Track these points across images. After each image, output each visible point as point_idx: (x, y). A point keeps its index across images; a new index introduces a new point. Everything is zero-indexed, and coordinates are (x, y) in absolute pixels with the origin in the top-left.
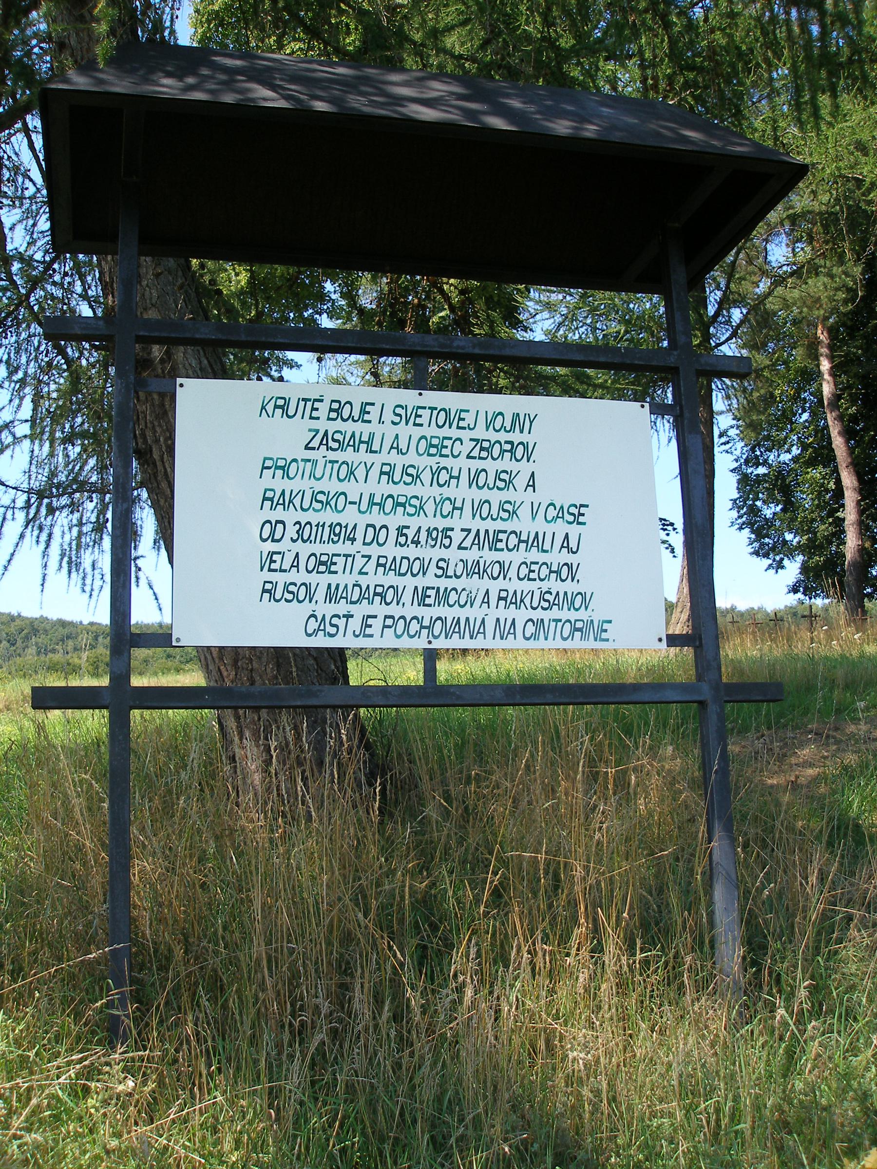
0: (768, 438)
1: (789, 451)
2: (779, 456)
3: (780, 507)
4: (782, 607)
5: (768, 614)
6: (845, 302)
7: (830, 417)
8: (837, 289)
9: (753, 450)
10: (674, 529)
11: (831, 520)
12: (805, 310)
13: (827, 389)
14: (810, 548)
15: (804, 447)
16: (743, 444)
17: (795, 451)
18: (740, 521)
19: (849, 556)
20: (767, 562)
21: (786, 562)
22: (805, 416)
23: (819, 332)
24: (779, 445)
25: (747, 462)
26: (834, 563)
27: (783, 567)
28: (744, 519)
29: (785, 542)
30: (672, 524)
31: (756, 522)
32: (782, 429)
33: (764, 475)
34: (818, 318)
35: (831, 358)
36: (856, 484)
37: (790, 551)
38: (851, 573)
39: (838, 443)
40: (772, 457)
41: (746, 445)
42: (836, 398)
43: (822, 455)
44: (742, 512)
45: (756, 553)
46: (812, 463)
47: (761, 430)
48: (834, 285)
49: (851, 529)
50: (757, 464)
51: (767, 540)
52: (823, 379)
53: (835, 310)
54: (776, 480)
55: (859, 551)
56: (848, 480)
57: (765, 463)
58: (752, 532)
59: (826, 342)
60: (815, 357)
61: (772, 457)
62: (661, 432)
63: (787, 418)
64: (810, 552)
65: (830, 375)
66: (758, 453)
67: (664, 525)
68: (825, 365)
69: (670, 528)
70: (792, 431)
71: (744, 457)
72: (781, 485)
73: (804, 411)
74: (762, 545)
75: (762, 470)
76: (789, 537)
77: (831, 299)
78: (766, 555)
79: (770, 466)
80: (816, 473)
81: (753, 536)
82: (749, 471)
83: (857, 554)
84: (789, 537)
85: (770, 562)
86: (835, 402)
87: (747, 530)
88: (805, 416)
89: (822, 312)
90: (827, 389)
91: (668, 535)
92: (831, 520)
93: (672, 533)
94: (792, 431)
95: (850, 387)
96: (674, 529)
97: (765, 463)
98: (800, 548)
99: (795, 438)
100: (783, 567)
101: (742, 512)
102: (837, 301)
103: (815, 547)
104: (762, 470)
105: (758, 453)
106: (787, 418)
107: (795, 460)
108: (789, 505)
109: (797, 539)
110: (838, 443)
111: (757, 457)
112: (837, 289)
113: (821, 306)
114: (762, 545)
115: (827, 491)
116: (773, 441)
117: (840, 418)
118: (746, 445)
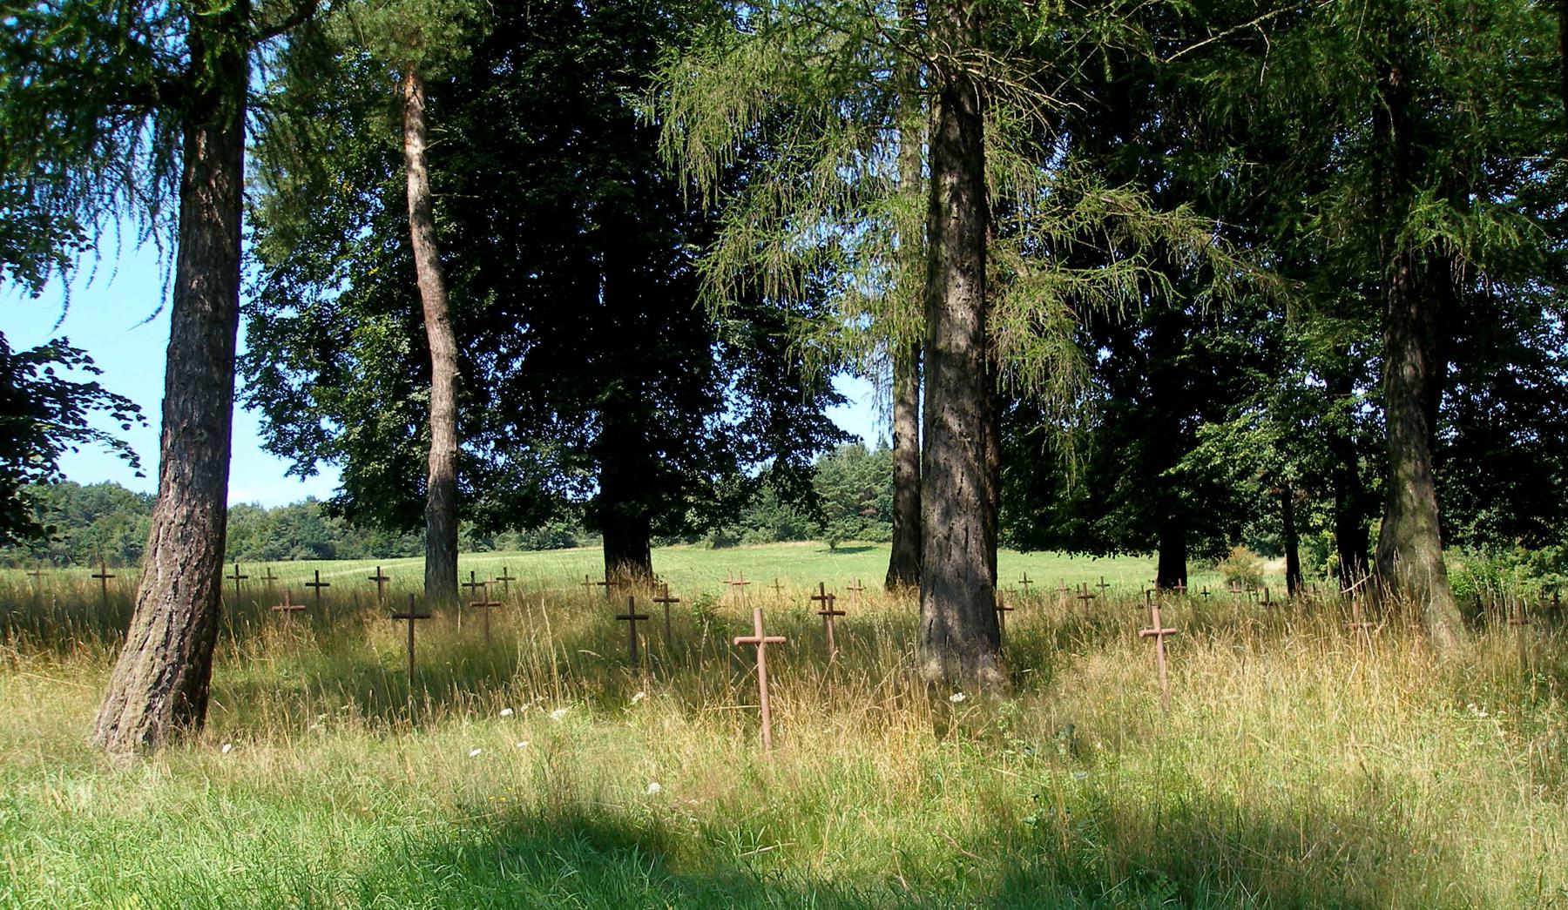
0: (301, 261)
1: (335, 285)
2: (319, 290)
3: (315, 374)
4: (286, 505)
5: (266, 515)
6: (463, 41)
7: (417, 235)
8: (448, 20)
9: (277, 278)
10: (140, 418)
11: (400, 404)
12: (393, 45)
13: (416, 187)
14: (363, 449)
15: (360, 281)
16: (261, 267)
17: (346, 285)
18: (249, 393)
19: (435, 469)
20: (288, 462)
21: (319, 464)
22: (367, 231)
23: (409, 90)
24: (318, 274)
25: (266, 296)
26: (406, 469)
27: (314, 472)
28: (255, 391)
29: (320, 434)
30: (136, 408)
31: (274, 396)
32: (326, 249)
33: (293, 321)
34: (413, 62)
35: (426, 136)
36: (453, 348)
37: (329, 450)
38: (437, 498)
39: (428, 279)
40: (307, 292)
41: (266, 269)
42: (429, 201)
43: (395, 291)
44: (253, 379)
45: (272, 447)
46: (375, 307)
47: (307, 237)
48: (445, 11)
49: (442, 424)
50: (283, 303)
51: (290, 427)
52: (409, 168)
53: (439, 55)
54: (312, 332)
55: (452, 461)
56: (440, 341)
57: (296, 301)
58: (267, 411)
59: (420, 108)
60: (398, 127)
61: (307, 293)
62: (125, 219)
63: (334, 232)
64: (361, 453)
65: (423, 164)
66: (286, 284)
67: (119, 407)
68: (415, 148)
69: (130, 414)
70: (343, 251)
71: (262, 288)
72: (320, 340)
73: (364, 222)
74: (282, 435)
75: (289, 313)
76: (326, 424)
77: (438, 34)
78: (288, 452)
79: (304, 308)
80: (382, 326)
81: (268, 419)
82: (269, 312)
83: (449, 467)
84: (326, 424)
85: (294, 462)
86: (424, 214)
87: (260, 409)
88: (367, 231)
89: (421, 54)
90: (416, 187)
91: (126, 427)
92: (400, 404)
93: (135, 425)
94: (343, 251)
95: (447, 188)
96: (140, 418)
97: (296, 301)
98: (346, 445)
99: (347, 264)
100: (314, 472)
101: (253, 379)
102: (448, 38)
103: (372, 446)
104: (289, 313)
105: (286, 284)
106: (336, 231)
107: (346, 299)
108: (332, 377)
109: (343, 430)
110: (428, 279)
111: (282, 290)
112: (448, 20)
113: (420, 43)
114: (282, 435)
115: (395, 354)
116: (311, 267)
117: (433, 237)
118: (266, 269)
